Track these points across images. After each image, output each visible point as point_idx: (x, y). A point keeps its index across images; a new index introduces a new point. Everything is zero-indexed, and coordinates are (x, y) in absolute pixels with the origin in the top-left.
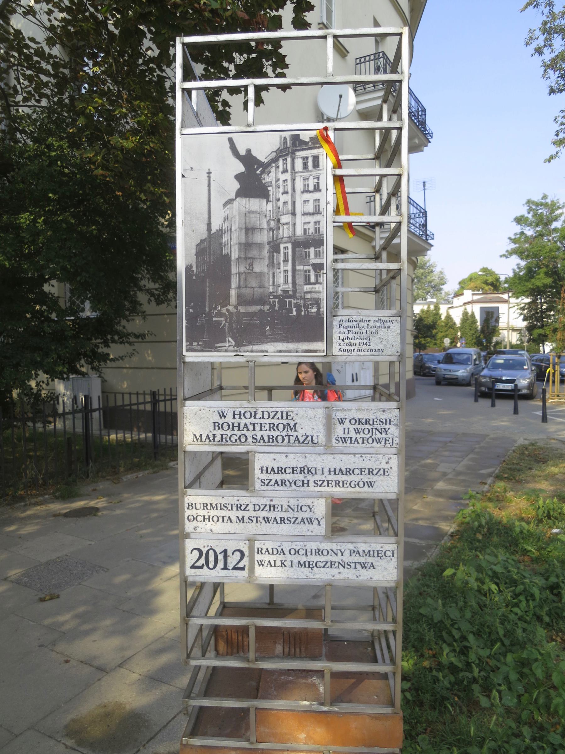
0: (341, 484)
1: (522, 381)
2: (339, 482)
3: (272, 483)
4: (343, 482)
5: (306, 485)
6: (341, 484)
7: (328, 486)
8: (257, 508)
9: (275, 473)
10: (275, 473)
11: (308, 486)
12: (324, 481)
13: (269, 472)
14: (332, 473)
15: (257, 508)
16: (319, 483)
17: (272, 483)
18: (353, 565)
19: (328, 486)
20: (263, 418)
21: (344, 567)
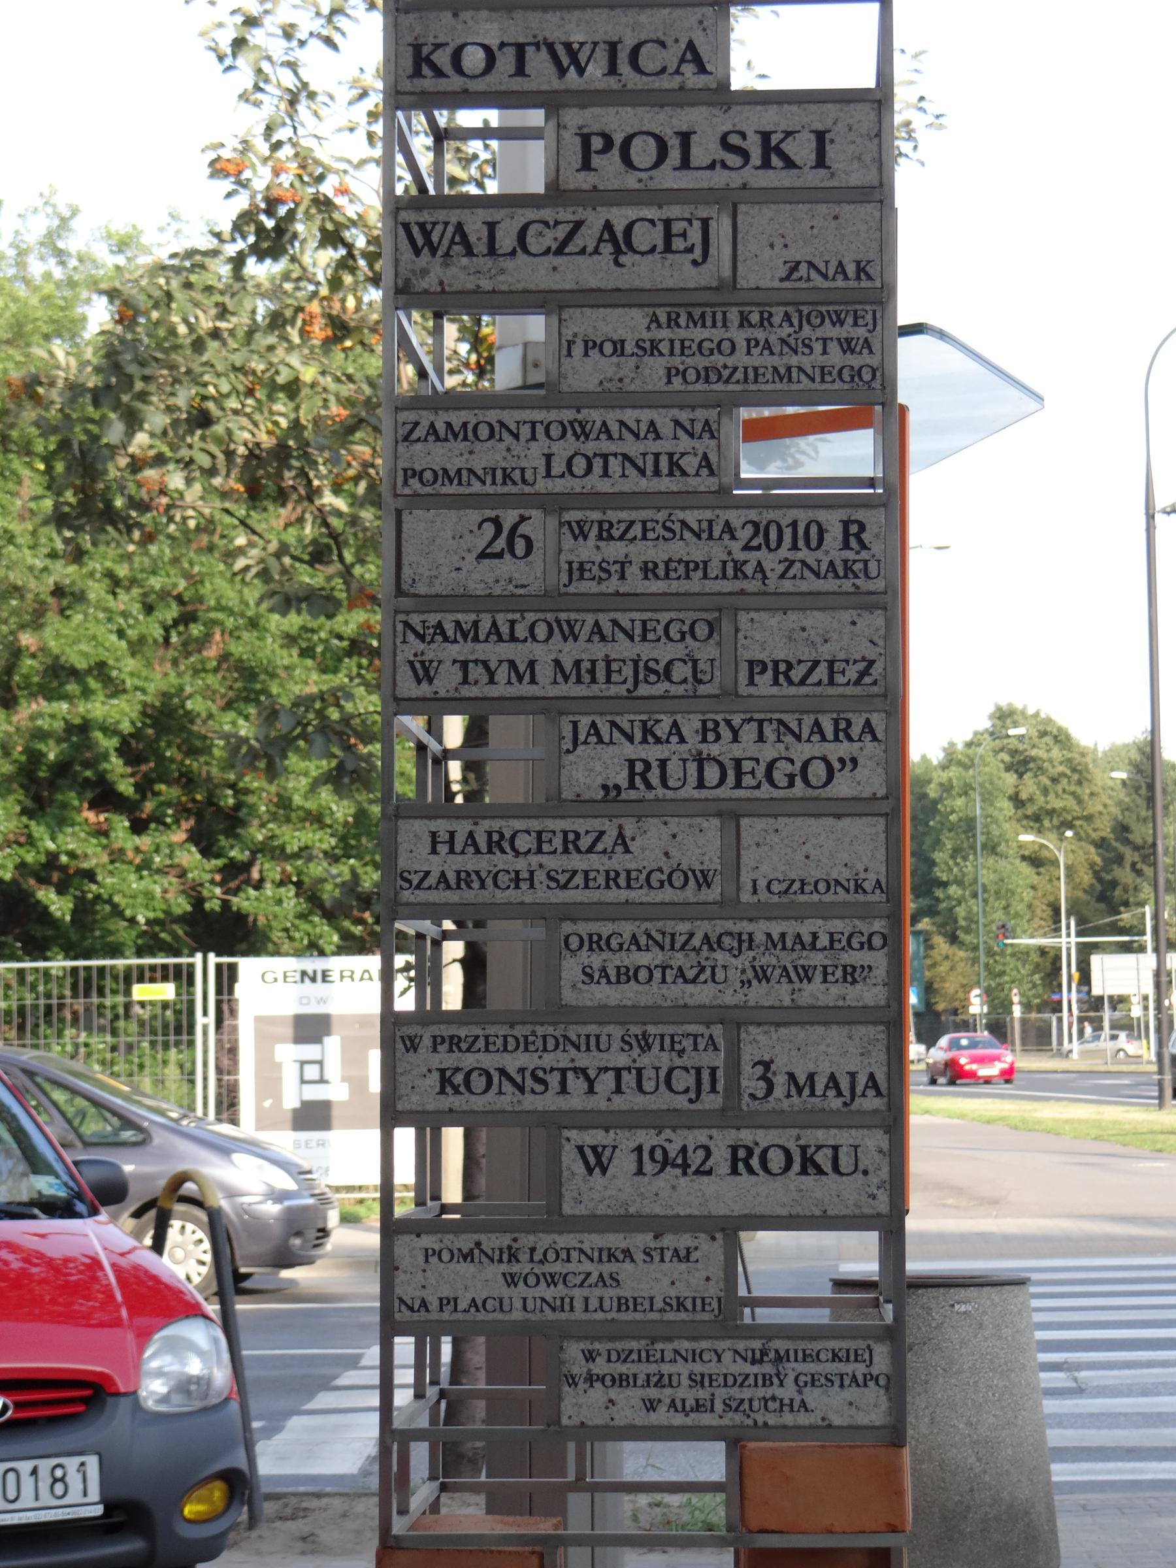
0: (622, 881)
1: (339, 816)
2: (618, 874)
3: (432, 880)
4: (629, 872)
5: (524, 886)
6: (622, 881)
7: (587, 887)
8: (730, 1380)
9: (478, 851)
10: (478, 851)
11: (532, 886)
12: (575, 872)
13: (458, 847)
14: (443, 849)
15: (730, 1380)
16: (563, 879)
17: (432, 880)
18: (554, 1080)
19: (587, 887)
20: (724, 576)
21: (521, 1089)
